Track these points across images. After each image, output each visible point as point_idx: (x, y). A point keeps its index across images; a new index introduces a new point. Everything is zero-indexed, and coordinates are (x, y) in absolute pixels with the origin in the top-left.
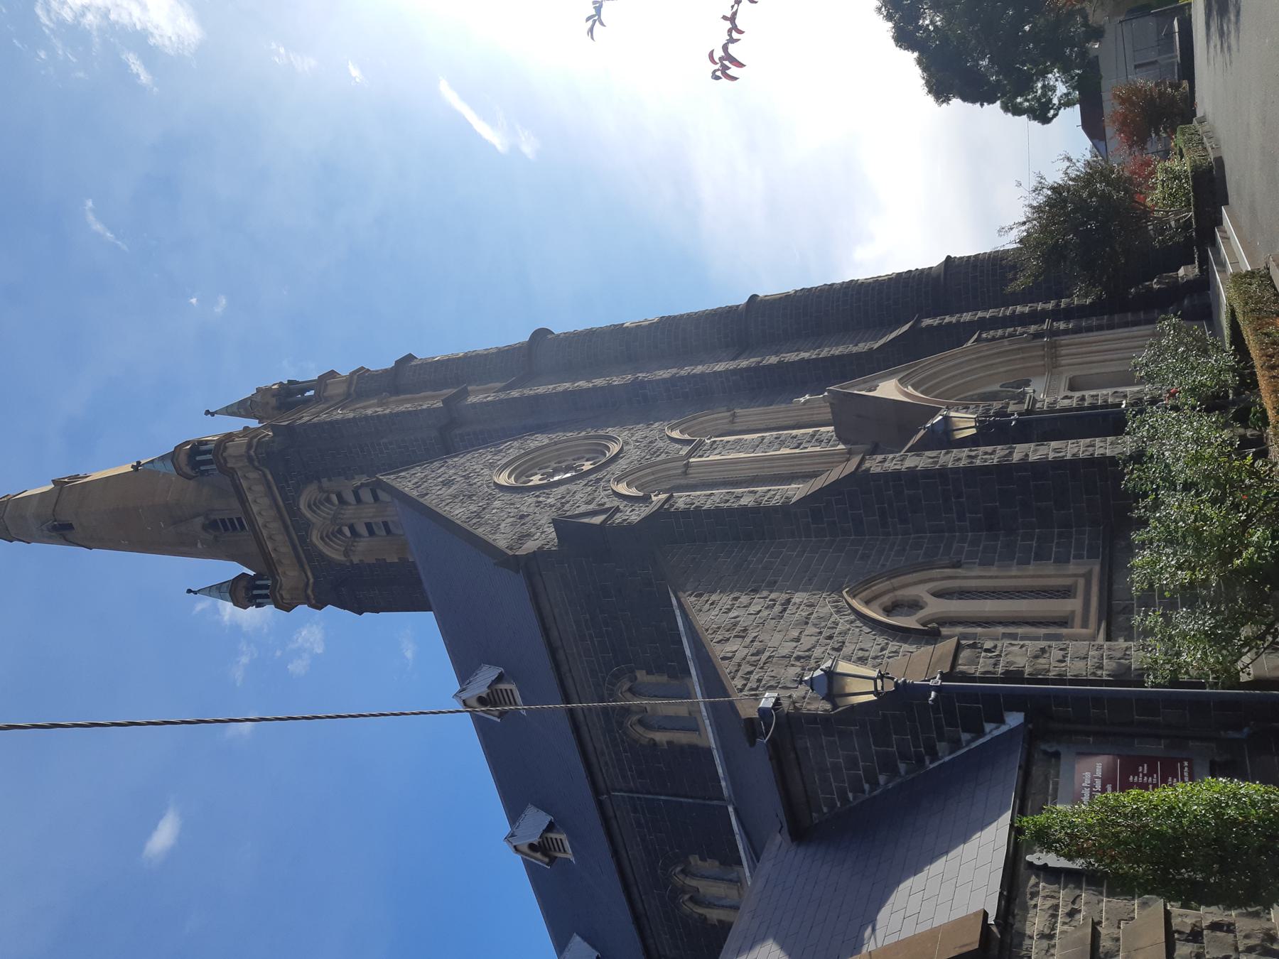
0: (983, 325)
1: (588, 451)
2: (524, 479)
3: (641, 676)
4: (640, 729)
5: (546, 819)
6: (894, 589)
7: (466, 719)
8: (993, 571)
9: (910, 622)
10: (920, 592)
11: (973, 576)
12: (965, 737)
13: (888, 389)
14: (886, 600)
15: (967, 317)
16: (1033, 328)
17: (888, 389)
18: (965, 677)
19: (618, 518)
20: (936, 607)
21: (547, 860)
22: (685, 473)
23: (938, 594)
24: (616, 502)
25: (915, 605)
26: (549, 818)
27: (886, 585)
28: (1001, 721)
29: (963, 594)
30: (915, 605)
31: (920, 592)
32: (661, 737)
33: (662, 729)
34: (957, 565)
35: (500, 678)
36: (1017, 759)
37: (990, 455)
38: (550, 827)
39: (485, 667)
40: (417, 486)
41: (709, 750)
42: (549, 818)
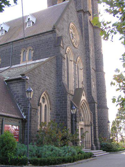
0: (94, 114)
1: (76, 41)
2: (71, 28)
3: (33, 52)
4: (23, 51)
5: (34, 22)
6: (47, 99)
7: (21, 16)
8: (49, 115)
9: (41, 101)
10: (46, 103)
11: (49, 112)
12: (22, 110)
13: (83, 98)
14: (45, 97)
15: (96, 111)
16: (92, 122)
17: (83, 98)
18: (31, 111)
19: (62, 49)
20: (43, 105)
21: (27, 22)
22: (70, 60)
23: (45, 106)
24: (65, 48)
25: (44, 102)
26: (7, 31)
27: (47, 97)
28: (25, 115)
29: (46, 110)
30: (44, 102)
31: (46, 103)
32: (22, 55)
33: (23, 54)
34: (50, 109)
35: (33, 23)
36: (18, 117)
37: (69, 116)
38: (6, 31)
39: (35, 19)
40: (71, 7)
41: (19, 63)
42: (7, 31)
